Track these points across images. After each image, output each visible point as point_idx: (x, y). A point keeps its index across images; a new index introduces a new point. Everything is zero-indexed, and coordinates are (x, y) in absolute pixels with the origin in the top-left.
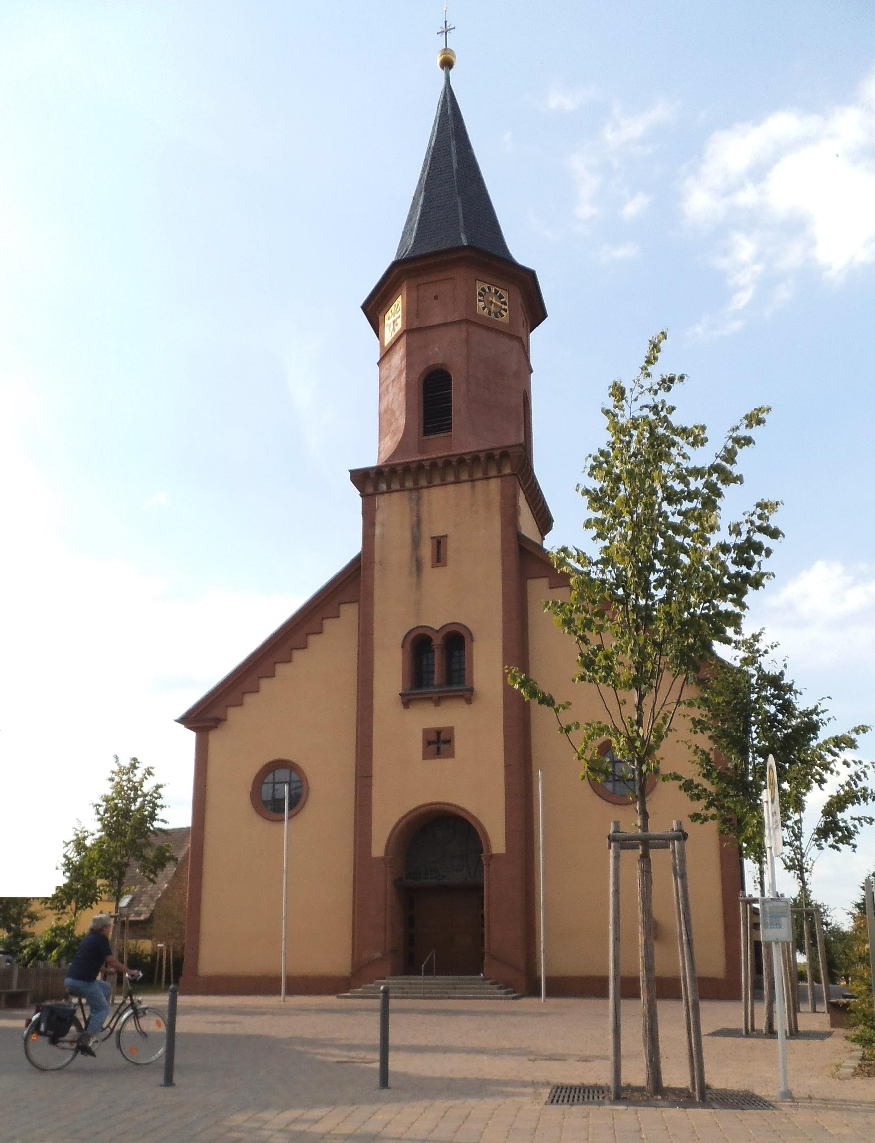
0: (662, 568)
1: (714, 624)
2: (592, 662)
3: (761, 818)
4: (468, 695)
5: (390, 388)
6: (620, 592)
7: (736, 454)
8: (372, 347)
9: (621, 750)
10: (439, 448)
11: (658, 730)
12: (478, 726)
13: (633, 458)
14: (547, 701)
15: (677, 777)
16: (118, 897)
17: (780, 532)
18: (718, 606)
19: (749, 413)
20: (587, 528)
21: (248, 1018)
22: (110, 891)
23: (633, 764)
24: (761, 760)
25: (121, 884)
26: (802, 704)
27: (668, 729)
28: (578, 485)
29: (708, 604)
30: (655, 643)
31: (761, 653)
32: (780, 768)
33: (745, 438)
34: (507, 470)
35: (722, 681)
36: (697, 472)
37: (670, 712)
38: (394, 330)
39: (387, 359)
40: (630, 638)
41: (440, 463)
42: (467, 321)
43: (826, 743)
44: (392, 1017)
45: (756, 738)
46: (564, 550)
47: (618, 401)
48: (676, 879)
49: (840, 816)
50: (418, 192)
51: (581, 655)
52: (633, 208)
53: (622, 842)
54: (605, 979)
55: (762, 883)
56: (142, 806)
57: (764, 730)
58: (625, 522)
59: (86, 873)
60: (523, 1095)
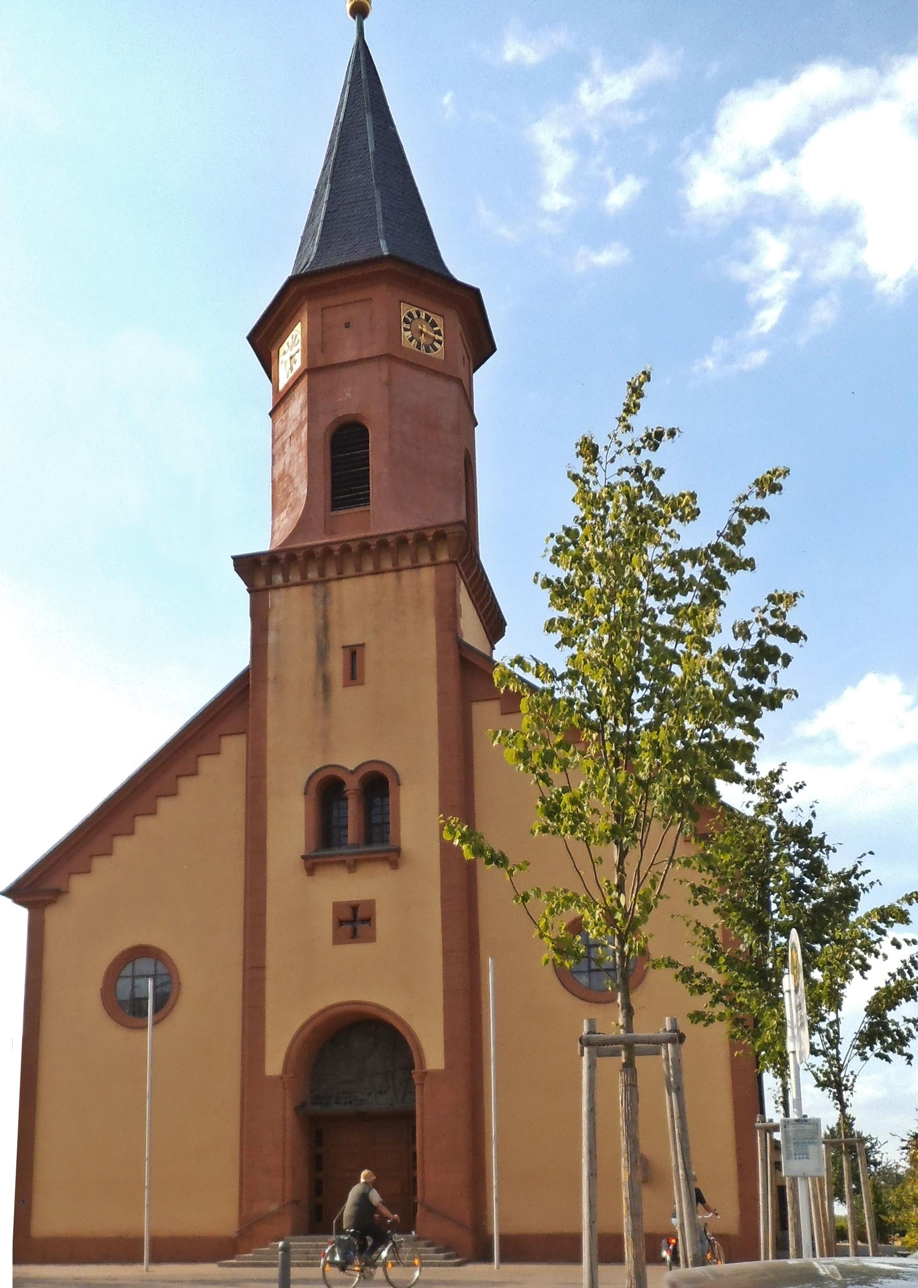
0: (647, 683)
1: (717, 756)
2: (557, 809)
3: (783, 1017)
4: (393, 857)
5: (287, 446)
6: (594, 716)
7: (744, 531)
9: (596, 925)
10: (352, 526)
11: (644, 898)
12: (407, 896)
13: (609, 539)
14: (499, 860)
15: (672, 964)
17: (801, 634)
18: (723, 734)
19: (760, 477)
20: (549, 631)
24: (782, 940)
26: (835, 864)
27: (659, 896)
28: (537, 575)
29: (708, 731)
30: (639, 782)
31: (782, 797)
32: (807, 949)
33: (755, 510)
34: (443, 557)
35: (731, 835)
36: (693, 556)
37: (661, 874)
38: (291, 369)
40: (605, 775)
41: (354, 546)
42: (389, 357)
43: (868, 916)
45: (776, 911)
46: (519, 661)
47: (589, 463)
48: (670, 1094)
49: (890, 1015)
50: (321, 184)
51: (543, 799)
52: (620, 196)
53: (598, 1046)
54: (578, 1238)
55: (785, 1104)
57: (787, 900)
58: (600, 624)
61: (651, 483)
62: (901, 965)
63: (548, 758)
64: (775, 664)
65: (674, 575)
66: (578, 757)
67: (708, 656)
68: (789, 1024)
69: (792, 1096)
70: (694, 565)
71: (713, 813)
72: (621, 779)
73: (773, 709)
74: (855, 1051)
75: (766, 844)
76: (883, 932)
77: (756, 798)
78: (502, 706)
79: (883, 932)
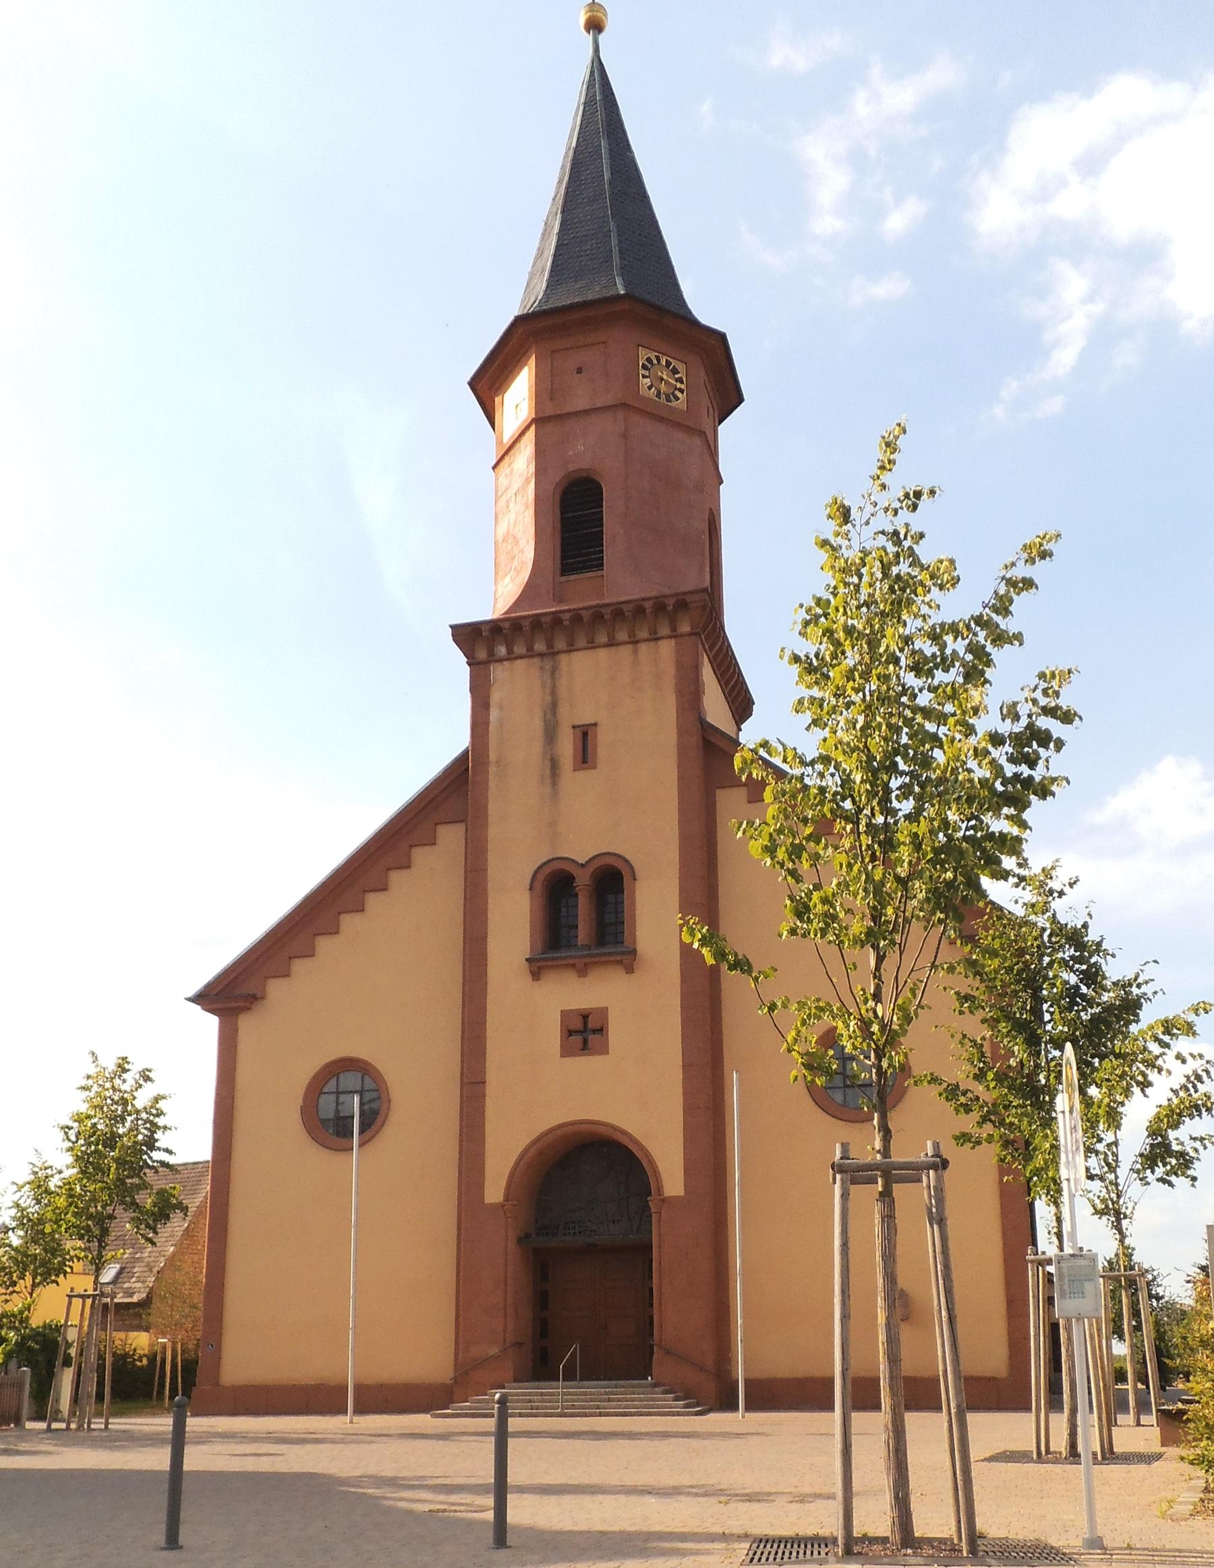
0: (907, 769)
1: (984, 851)
2: (807, 908)
3: (1056, 1139)
5: (512, 505)
6: (848, 804)
8: (485, 443)
9: (850, 1037)
10: (583, 593)
12: (643, 1006)
13: (864, 609)
15: (934, 1080)
16: (98, 1266)
17: (1075, 714)
21: (296, 1448)
22: (86, 1257)
23: (868, 1058)
24: (1057, 1053)
25: (101, 1247)
26: (1114, 970)
27: (920, 1006)
29: (973, 822)
30: (898, 879)
32: (1083, 1063)
33: (1024, 580)
34: (685, 628)
36: (954, 629)
39: (507, 459)
40: (859, 871)
41: (586, 615)
42: (625, 406)
43: (1151, 1028)
44: (512, 1443)
45: (1049, 1022)
46: (765, 744)
49: (1172, 1135)
51: (791, 898)
52: (897, 222)
53: (853, 1173)
54: (831, 1381)
55: (1059, 1235)
56: (135, 1129)
58: (854, 703)
59: (48, 1230)
60: (708, 1552)
61: (910, 548)
62: (1184, 1080)
63: (796, 852)
64: (1047, 748)
65: (935, 649)
66: (830, 850)
67: (973, 740)
68: (1062, 1149)
69: (1066, 1227)
70: (956, 638)
71: (982, 913)
72: (878, 875)
73: (1044, 798)
74: (1135, 1175)
75: (1038, 947)
76: (1167, 1046)
77: (1028, 895)
78: (749, 794)
79: (1167, 1046)
